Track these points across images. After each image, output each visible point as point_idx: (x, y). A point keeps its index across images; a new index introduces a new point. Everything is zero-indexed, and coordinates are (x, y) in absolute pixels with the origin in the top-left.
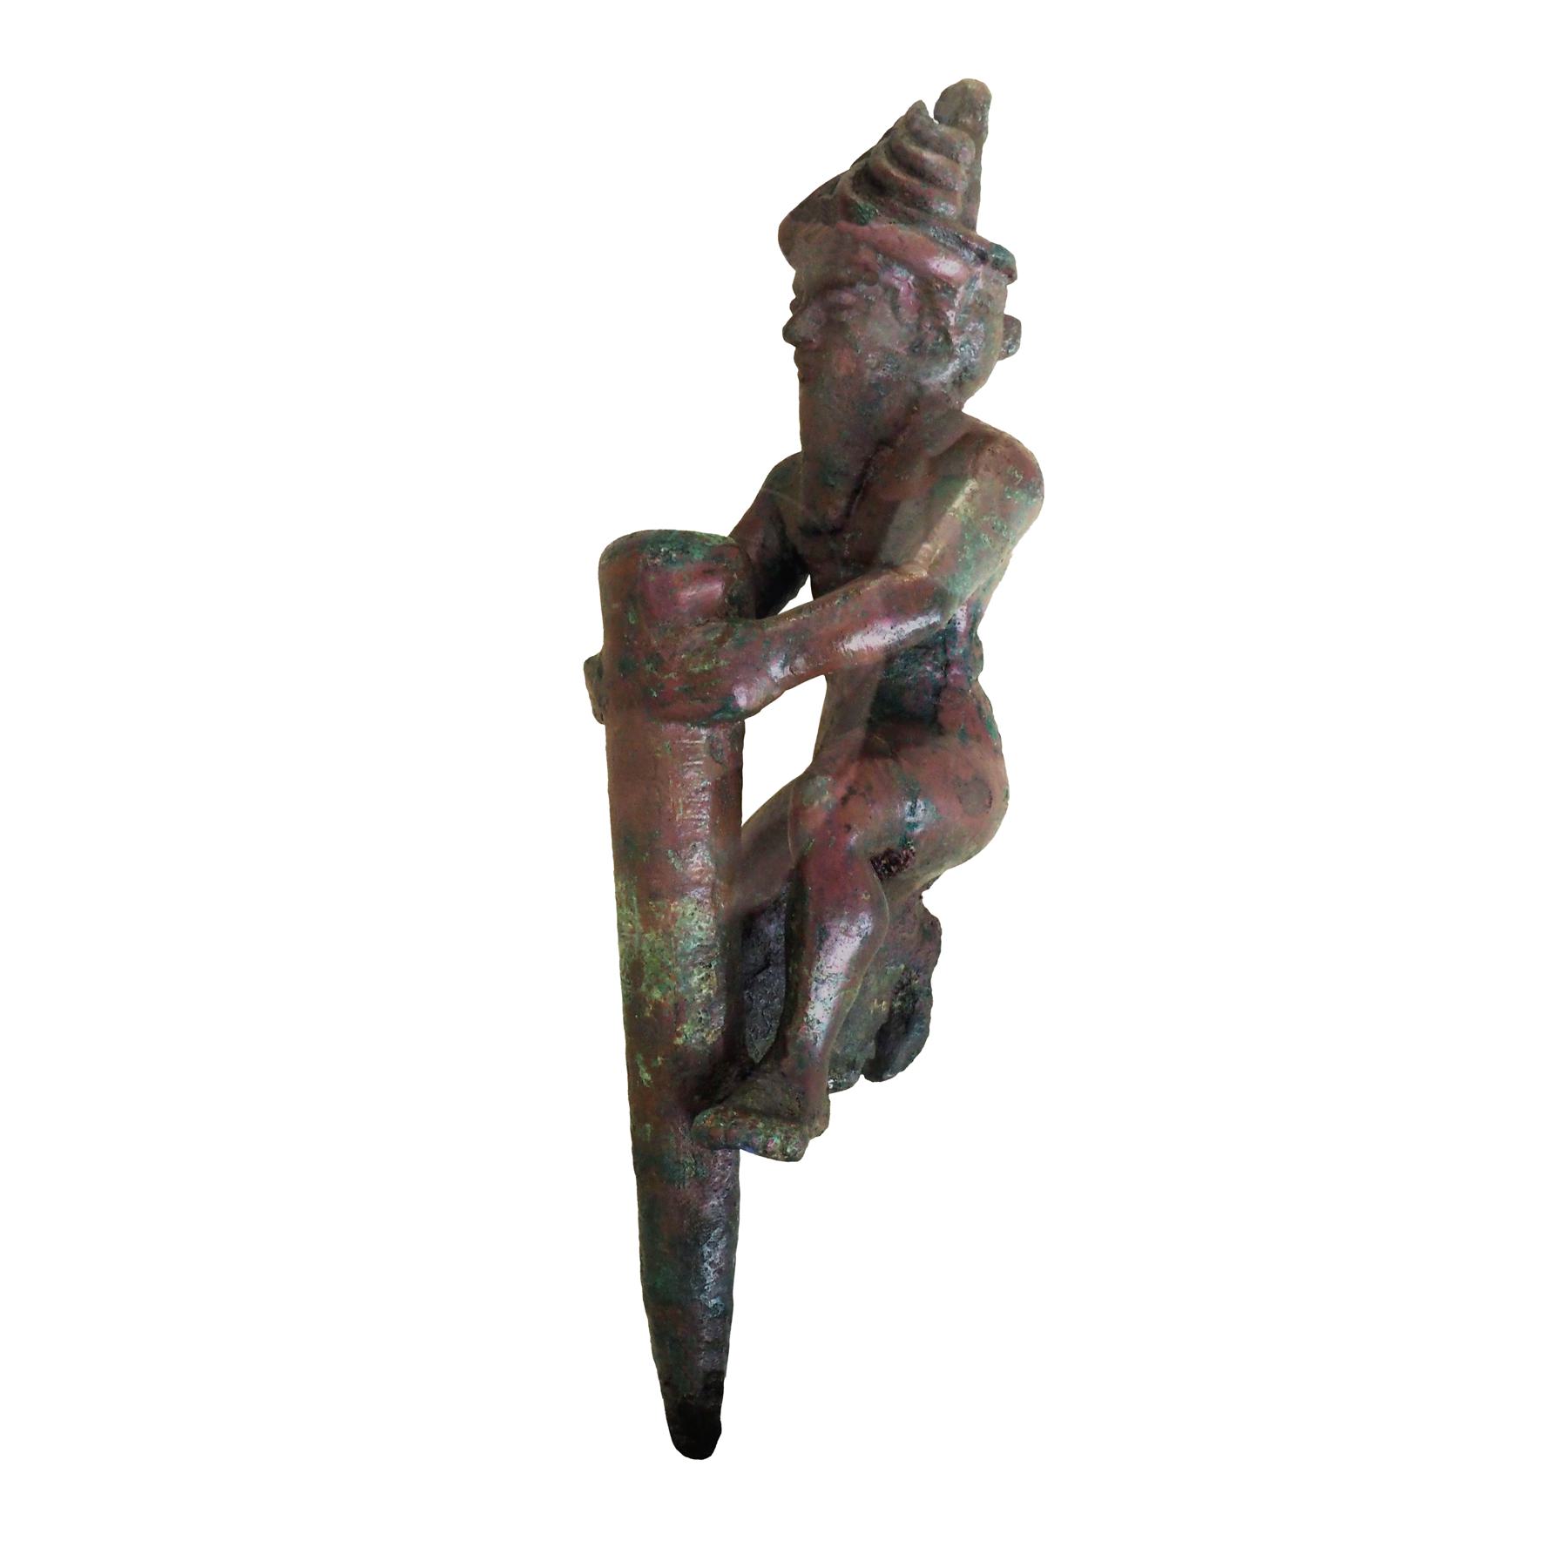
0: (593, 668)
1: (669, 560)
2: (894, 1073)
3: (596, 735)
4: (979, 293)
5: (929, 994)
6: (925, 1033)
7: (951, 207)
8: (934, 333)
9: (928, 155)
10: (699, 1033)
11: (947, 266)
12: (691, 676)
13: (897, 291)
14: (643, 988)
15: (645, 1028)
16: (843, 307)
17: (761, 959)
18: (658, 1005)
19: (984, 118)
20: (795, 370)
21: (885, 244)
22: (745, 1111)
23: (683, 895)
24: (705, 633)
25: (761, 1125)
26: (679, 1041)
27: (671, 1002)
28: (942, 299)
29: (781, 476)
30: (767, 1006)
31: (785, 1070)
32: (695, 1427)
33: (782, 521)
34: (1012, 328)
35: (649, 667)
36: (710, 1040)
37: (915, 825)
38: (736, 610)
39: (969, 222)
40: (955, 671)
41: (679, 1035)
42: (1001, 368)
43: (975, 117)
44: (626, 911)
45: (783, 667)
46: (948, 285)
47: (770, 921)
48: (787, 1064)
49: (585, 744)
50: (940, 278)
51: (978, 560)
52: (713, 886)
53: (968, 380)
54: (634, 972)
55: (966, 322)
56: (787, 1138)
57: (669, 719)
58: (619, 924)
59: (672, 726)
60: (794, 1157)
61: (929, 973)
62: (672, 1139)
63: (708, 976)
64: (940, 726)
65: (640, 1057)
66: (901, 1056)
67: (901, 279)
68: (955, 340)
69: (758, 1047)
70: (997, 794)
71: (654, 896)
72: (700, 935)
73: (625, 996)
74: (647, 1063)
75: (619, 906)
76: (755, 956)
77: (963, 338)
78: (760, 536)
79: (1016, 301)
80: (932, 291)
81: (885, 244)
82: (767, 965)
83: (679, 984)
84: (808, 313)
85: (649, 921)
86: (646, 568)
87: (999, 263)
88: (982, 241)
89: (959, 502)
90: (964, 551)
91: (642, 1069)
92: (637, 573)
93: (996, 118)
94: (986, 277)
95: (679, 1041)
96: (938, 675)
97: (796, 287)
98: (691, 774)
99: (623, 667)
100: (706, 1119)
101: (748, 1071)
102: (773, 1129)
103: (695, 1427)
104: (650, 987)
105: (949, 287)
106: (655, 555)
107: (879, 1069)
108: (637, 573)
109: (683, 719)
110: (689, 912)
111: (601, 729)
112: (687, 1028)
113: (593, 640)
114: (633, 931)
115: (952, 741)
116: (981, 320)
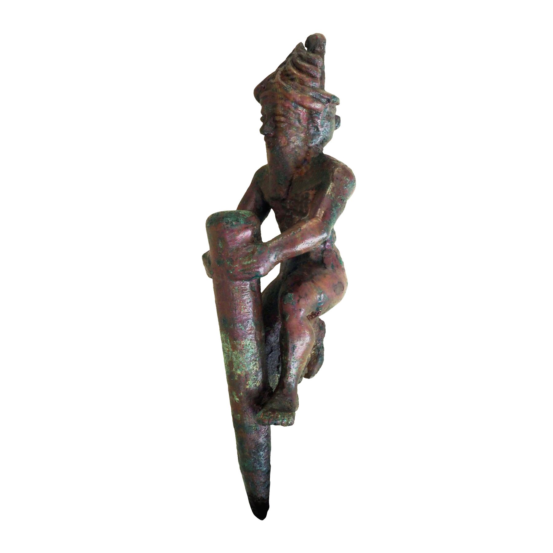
0: (205, 257)
1: (232, 225)
2: (314, 376)
3: (210, 282)
4: (328, 112)
5: (323, 347)
6: (322, 360)
7: (317, 84)
8: (313, 128)
9: (303, 64)
10: (253, 383)
11: (317, 106)
12: (244, 266)
13: (299, 114)
14: (234, 370)
15: (234, 383)
16: (281, 122)
17: (270, 349)
18: (239, 375)
19: (324, 48)
20: (265, 143)
21: (293, 92)
22: (273, 411)
23: (245, 339)
24: (247, 250)
25: (280, 416)
26: (248, 387)
27: (244, 374)
28: (316, 117)
29: (260, 174)
30: (273, 364)
31: (285, 393)
32: (260, 507)
33: (261, 192)
34: (338, 119)
35: (228, 263)
36: (258, 385)
37: (321, 303)
38: (256, 239)
39: (322, 87)
40: (328, 244)
41: (247, 385)
42: (336, 133)
43: (321, 48)
44: (225, 344)
45: (275, 258)
46: (317, 112)
47: (272, 336)
48: (285, 391)
49: (206, 286)
50: (314, 110)
51: (337, 212)
52: (255, 333)
53: (324, 142)
54: (230, 365)
55: (324, 123)
56: (289, 419)
57: (236, 280)
58: (223, 348)
59: (238, 282)
60: (291, 424)
61: (322, 341)
62: (247, 419)
63: (256, 364)
64: (325, 264)
65: (234, 393)
66: (316, 369)
67: (302, 112)
68: (320, 129)
69: (274, 382)
70: (345, 286)
71: (235, 340)
72: (253, 350)
73: (227, 372)
74: (237, 395)
75: (223, 342)
76: (268, 349)
77: (323, 129)
78: (254, 197)
79: (339, 111)
80: (312, 114)
81: (293, 92)
82: (272, 351)
83: (246, 368)
84: (268, 124)
85: (234, 348)
86: (225, 229)
87: (332, 100)
88: (328, 95)
89: (329, 191)
90: (333, 210)
91: (236, 397)
92: (217, 224)
93: (328, 48)
94: (330, 106)
95: (248, 387)
96: (322, 246)
97: (262, 112)
98: (246, 297)
99: (219, 262)
100: (260, 414)
101: (272, 394)
102: (284, 417)
103: (260, 507)
104: (236, 370)
105: (318, 112)
106: (227, 223)
107: (309, 375)
108: (217, 224)
109: (241, 280)
110: (248, 344)
111: (211, 280)
112: (250, 382)
113: (206, 248)
114: (228, 351)
115: (330, 269)
116: (329, 121)
